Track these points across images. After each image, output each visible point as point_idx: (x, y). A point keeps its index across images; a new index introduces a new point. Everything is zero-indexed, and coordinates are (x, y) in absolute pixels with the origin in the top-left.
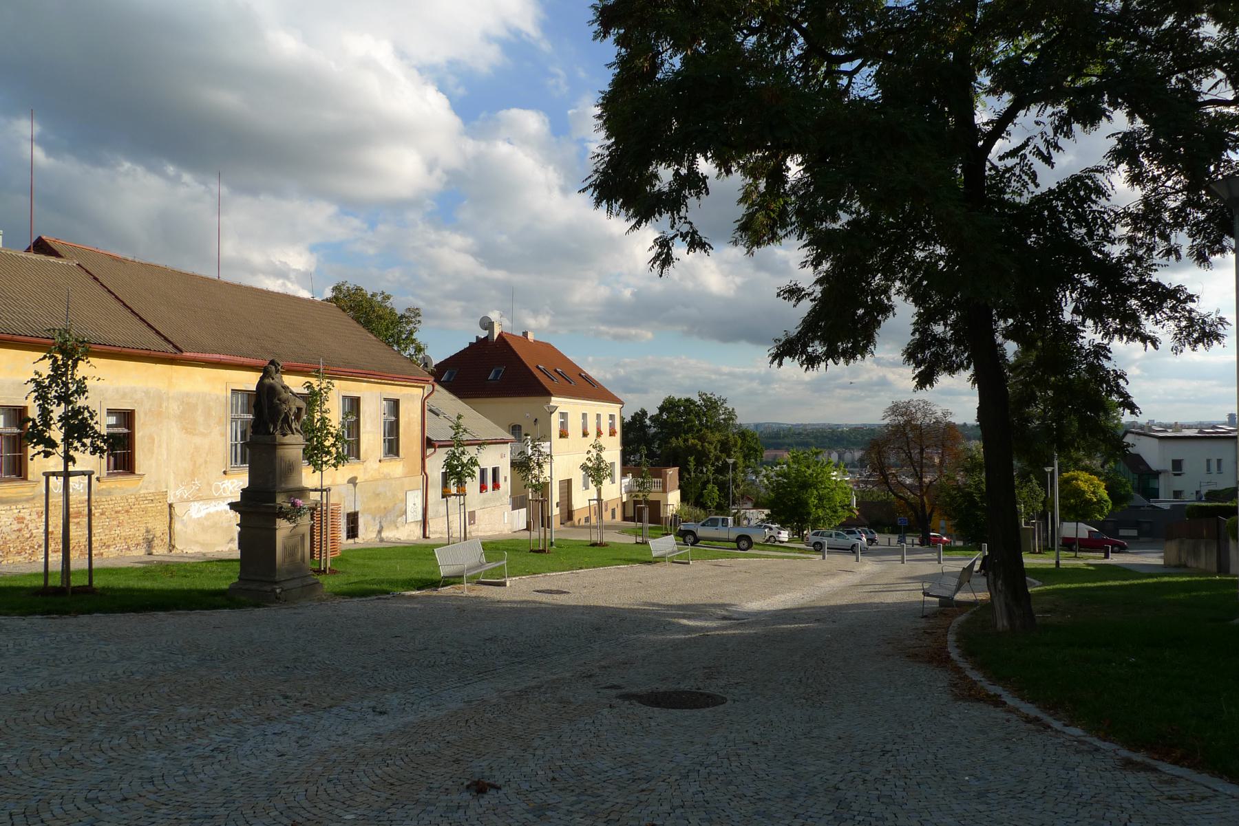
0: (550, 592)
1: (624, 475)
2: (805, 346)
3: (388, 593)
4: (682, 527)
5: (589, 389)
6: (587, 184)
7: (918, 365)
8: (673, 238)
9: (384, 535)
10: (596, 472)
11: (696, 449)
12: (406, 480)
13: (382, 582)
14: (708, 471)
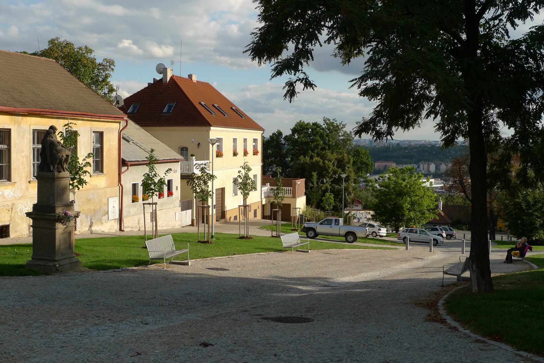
0: (217, 269)
1: (263, 184)
2: (375, 125)
3: (119, 268)
4: (306, 225)
5: (237, 118)
6: (248, 48)
7: (445, 133)
8: (295, 82)
9: (93, 228)
10: (244, 185)
11: (319, 165)
12: (108, 189)
13: (113, 261)
14: (327, 182)
